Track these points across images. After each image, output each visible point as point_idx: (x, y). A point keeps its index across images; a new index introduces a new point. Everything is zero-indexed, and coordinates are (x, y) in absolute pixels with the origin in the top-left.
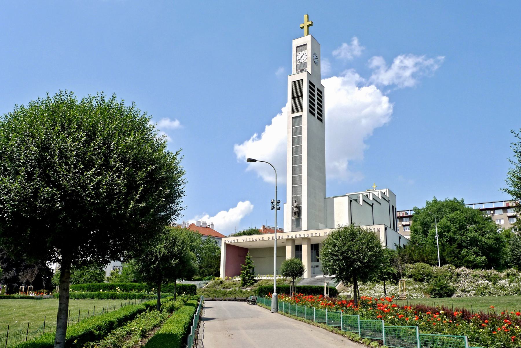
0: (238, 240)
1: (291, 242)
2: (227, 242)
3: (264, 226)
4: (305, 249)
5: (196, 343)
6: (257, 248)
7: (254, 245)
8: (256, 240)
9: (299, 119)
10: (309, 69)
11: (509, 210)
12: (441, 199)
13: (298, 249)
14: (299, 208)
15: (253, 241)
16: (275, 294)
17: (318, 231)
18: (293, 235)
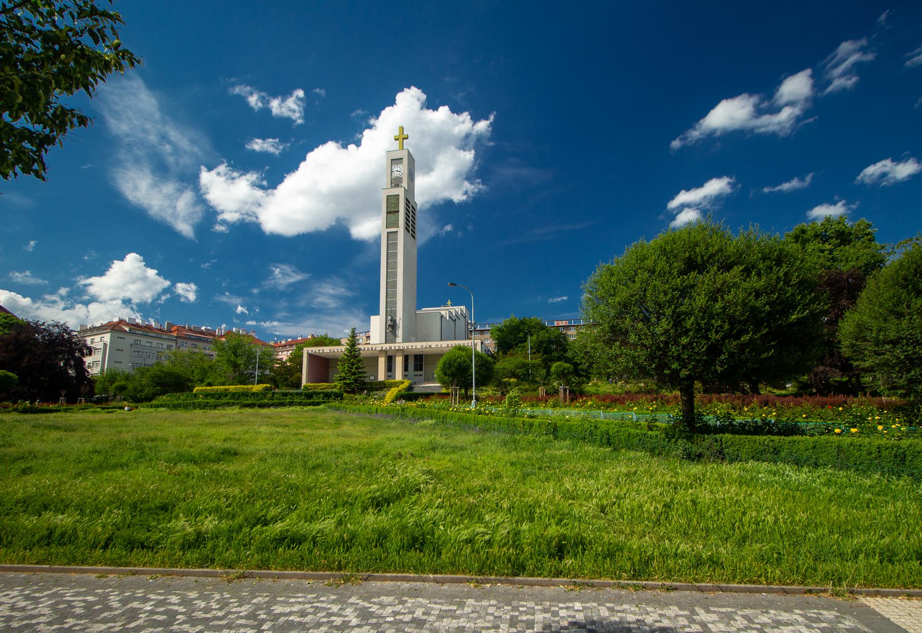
1: (384, 354)
2: (310, 352)
4: (399, 361)
7: (429, 351)
8: (315, 352)
10: (405, 184)
12: (329, 336)
13: (390, 360)
14: (394, 321)
16: (474, 401)
18: (387, 346)
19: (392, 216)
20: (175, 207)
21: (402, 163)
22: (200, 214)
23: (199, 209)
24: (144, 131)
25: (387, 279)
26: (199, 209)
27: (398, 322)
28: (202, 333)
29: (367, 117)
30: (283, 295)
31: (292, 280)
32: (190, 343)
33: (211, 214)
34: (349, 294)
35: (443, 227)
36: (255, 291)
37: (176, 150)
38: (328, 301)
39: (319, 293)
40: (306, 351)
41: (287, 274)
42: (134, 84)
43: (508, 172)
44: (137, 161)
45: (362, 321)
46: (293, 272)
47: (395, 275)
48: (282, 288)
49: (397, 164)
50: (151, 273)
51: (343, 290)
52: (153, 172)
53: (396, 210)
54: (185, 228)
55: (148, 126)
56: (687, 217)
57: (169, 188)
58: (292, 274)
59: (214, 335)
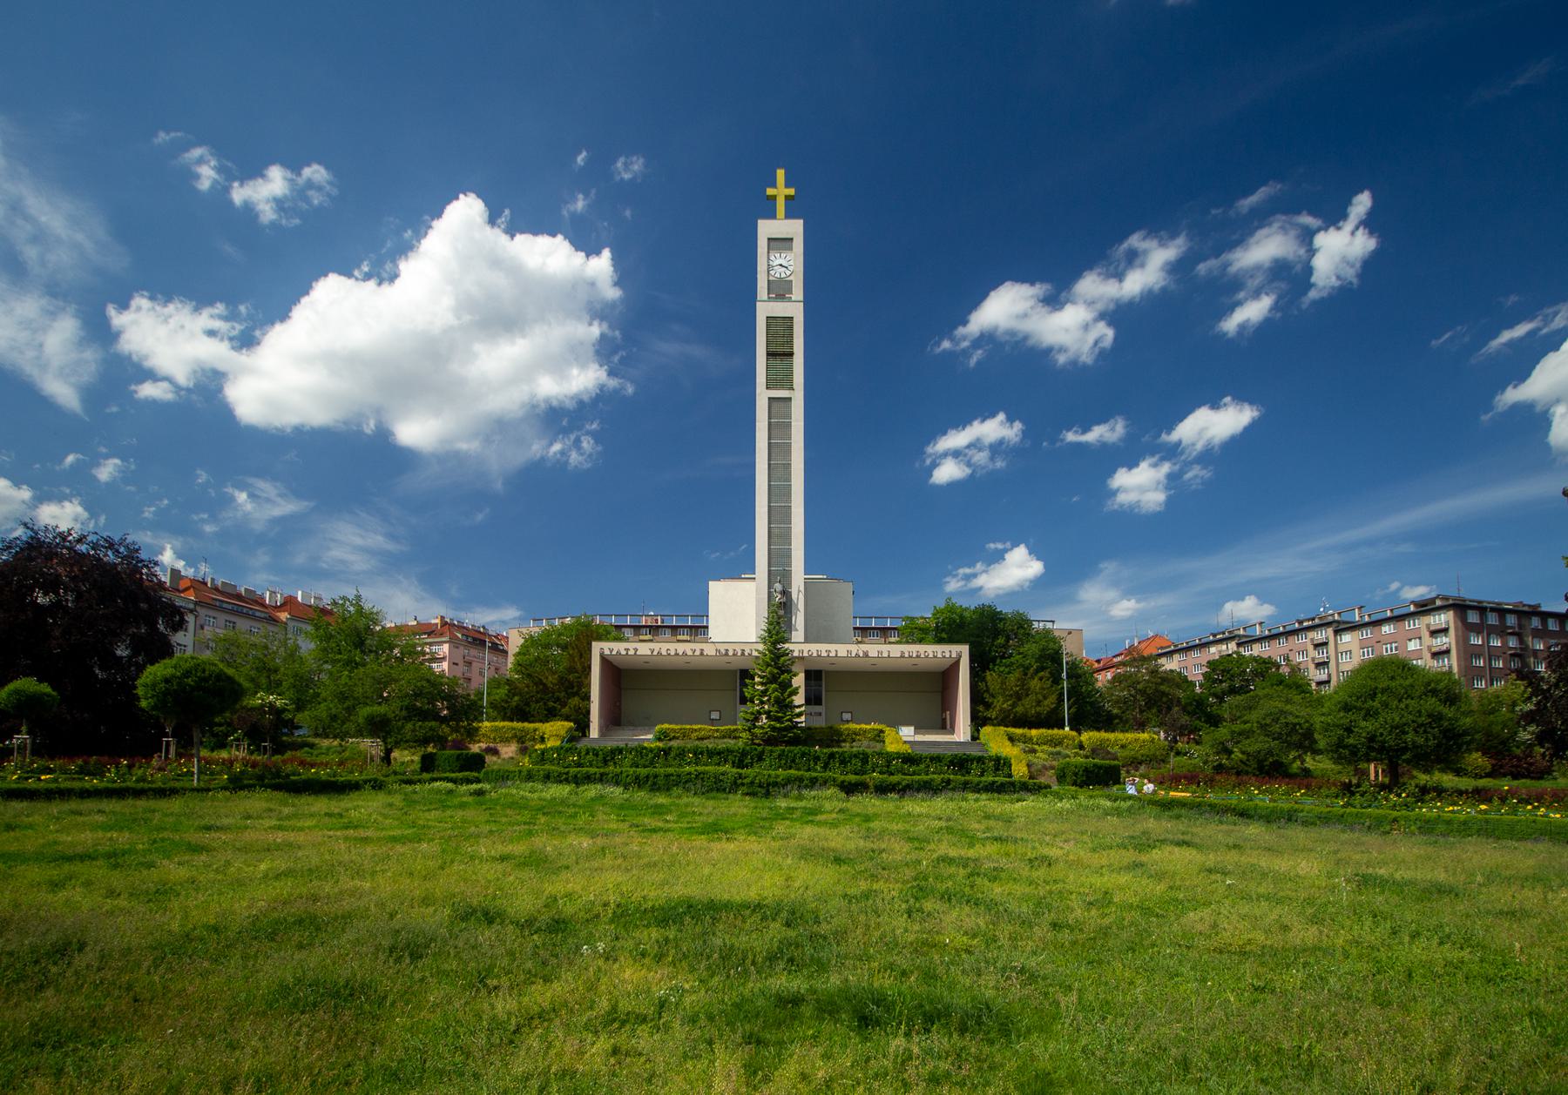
0: (636, 650)
2: (607, 652)
3: (442, 618)
6: (837, 672)
8: (685, 654)
9: (782, 404)
17: (833, 647)
19: (777, 362)
20: (41, 345)
22: (93, 367)
23: (91, 355)
25: (769, 502)
26: (91, 355)
27: (794, 596)
28: (239, 597)
31: (277, 512)
32: (222, 617)
34: (391, 546)
35: (551, 444)
37: (40, 237)
38: (351, 557)
39: (333, 540)
40: (597, 647)
41: (268, 500)
43: (667, 349)
46: (280, 495)
48: (258, 527)
49: (780, 250)
51: (380, 538)
54: (63, 392)
56: (947, 472)
58: (279, 499)
59: (263, 605)
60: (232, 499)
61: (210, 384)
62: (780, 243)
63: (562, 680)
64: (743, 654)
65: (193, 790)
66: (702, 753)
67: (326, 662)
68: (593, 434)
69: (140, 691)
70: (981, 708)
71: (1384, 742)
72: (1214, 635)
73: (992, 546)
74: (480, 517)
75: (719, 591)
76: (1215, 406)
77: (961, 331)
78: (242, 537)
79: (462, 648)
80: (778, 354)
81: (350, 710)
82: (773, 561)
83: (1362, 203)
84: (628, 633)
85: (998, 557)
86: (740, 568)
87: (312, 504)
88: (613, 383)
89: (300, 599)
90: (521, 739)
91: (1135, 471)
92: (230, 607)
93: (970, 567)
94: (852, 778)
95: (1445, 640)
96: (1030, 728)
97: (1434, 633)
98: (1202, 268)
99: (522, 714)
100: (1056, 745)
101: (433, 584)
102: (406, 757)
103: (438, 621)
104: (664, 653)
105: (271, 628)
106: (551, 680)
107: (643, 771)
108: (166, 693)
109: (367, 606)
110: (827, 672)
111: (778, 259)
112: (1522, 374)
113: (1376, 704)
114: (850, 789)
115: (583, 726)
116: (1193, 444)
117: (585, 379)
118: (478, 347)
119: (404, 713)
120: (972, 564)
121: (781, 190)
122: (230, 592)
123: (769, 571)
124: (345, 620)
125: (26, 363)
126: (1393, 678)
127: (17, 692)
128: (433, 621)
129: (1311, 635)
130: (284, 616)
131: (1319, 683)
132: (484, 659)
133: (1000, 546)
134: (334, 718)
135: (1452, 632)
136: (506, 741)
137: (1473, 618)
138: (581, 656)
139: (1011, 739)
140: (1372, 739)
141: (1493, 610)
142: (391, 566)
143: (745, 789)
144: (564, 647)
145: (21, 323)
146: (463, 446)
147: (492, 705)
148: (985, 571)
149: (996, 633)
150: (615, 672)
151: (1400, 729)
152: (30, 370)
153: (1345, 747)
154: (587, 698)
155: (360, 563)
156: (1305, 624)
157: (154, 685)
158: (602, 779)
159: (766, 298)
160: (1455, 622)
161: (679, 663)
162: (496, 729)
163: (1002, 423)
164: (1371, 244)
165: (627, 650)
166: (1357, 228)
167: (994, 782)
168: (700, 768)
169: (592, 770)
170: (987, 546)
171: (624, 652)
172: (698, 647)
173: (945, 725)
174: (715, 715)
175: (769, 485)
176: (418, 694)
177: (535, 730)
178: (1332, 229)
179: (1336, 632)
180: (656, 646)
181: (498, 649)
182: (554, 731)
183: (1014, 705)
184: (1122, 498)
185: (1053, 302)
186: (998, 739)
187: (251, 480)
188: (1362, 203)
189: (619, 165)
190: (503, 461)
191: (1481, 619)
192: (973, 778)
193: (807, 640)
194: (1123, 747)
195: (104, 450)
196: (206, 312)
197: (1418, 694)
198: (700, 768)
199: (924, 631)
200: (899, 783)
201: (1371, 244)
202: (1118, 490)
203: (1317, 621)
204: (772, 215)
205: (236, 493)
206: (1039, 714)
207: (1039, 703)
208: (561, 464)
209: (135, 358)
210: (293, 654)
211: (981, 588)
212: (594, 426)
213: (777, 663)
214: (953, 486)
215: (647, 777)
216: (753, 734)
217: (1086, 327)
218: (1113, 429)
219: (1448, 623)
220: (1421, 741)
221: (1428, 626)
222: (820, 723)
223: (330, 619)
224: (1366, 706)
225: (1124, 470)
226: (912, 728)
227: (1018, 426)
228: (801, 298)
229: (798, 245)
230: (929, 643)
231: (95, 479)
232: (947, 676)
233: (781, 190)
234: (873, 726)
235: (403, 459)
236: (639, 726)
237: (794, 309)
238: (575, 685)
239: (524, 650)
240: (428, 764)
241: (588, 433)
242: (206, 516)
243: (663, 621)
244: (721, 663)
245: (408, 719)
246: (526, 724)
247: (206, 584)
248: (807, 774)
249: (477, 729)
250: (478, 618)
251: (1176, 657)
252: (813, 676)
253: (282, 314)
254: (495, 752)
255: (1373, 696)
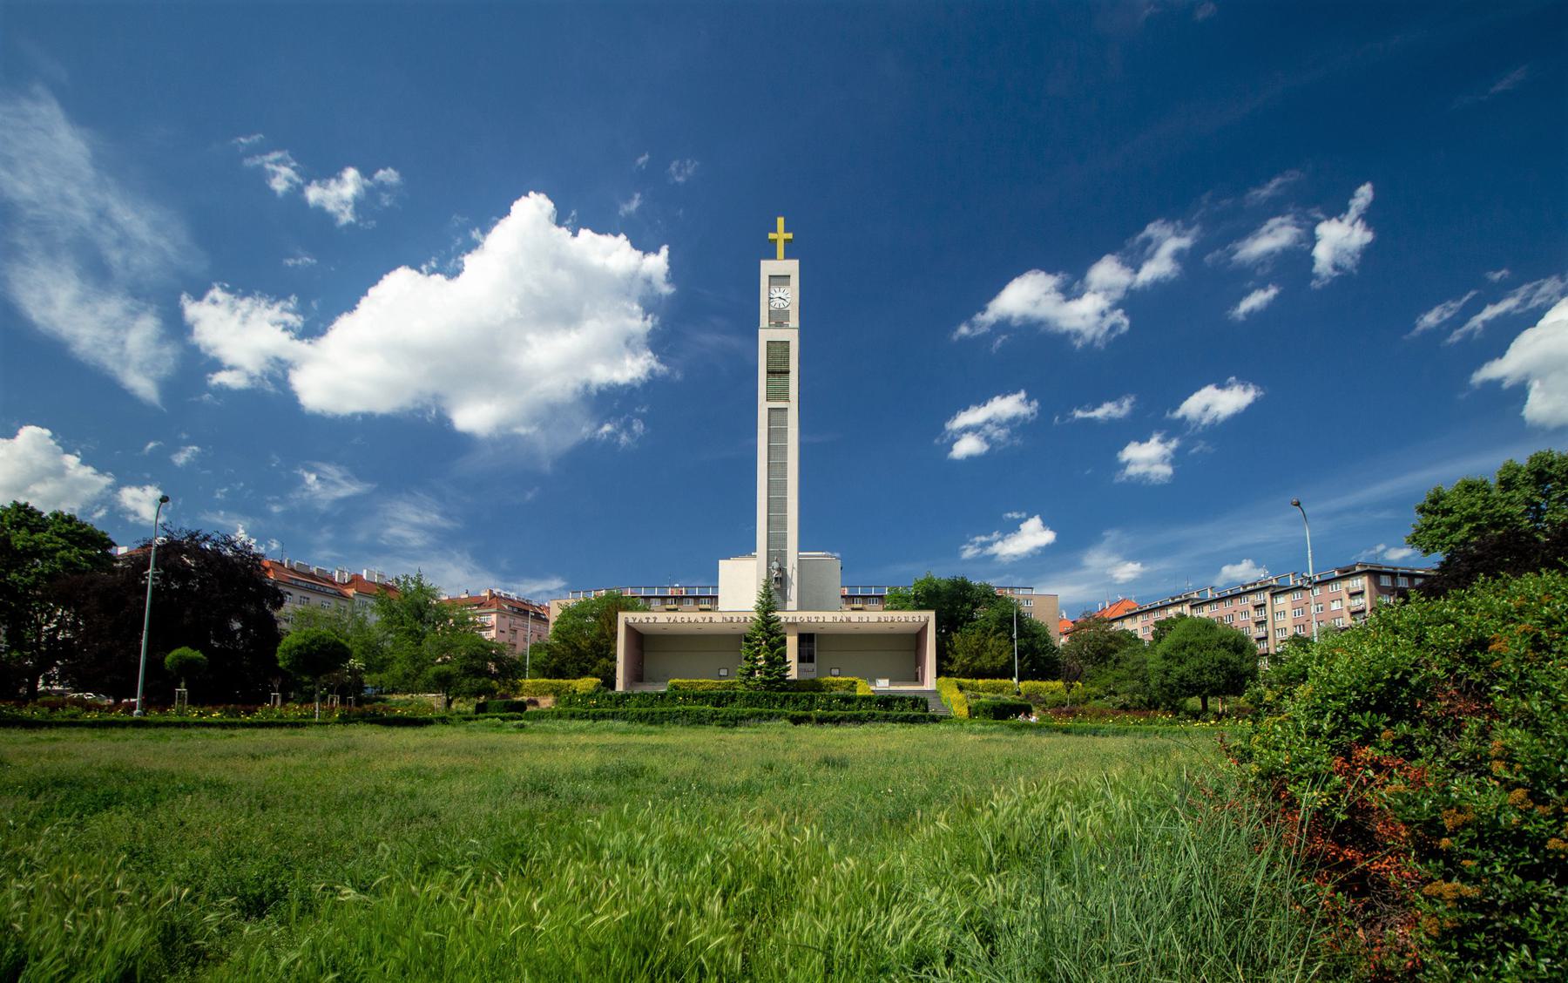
0: (655, 618)
2: (631, 621)
3: (491, 591)
5: (1215, 869)
6: (832, 635)
8: (641, 621)
11: (669, 600)
15: (690, 622)
19: (776, 379)
20: (123, 343)
21: (788, 284)
22: (171, 362)
23: (170, 351)
24: (65, 201)
26: (170, 351)
27: (789, 573)
28: (312, 576)
29: (465, 230)
30: (325, 518)
33: (198, 364)
34: (446, 524)
35: (601, 426)
36: (276, 509)
37: (124, 241)
39: (394, 519)
40: (623, 617)
41: (333, 483)
42: (44, 110)
44: (51, 251)
45: (469, 573)
46: (345, 478)
47: (783, 487)
48: (323, 507)
50: (72, 461)
51: (436, 517)
52: (82, 276)
53: (784, 369)
54: (143, 385)
55: (73, 191)
56: (967, 447)
57: (113, 307)
58: (342, 482)
59: (333, 583)
60: (302, 480)
61: (279, 371)
62: (780, 280)
63: (593, 645)
64: (745, 621)
65: (317, 724)
66: (689, 697)
67: (390, 632)
68: (645, 419)
69: (279, 655)
70: (945, 663)
71: (1189, 681)
72: (1173, 599)
73: (1009, 515)
74: (529, 496)
75: (727, 568)
76: (1222, 386)
77: (979, 317)
78: (310, 517)
79: (508, 617)
80: (778, 371)
81: (420, 670)
82: (771, 543)
83: (1364, 194)
84: (656, 604)
85: (1013, 528)
86: (745, 548)
87: (375, 486)
88: (662, 369)
89: (365, 577)
90: (556, 692)
91: (1145, 445)
92: (305, 585)
93: (986, 536)
94: (801, 713)
95: (1361, 601)
96: (977, 679)
97: (1352, 595)
98: (1208, 259)
99: (559, 673)
100: (998, 692)
101: (484, 559)
102: (463, 706)
103: (486, 594)
104: (679, 621)
105: (343, 603)
106: (584, 644)
107: (644, 710)
108: (298, 656)
109: (426, 582)
110: (821, 636)
111: (778, 292)
112: (1500, 352)
113: (1185, 654)
114: (797, 721)
115: (610, 682)
116: (1201, 419)
117: (633, 368)
118: (530, 337)
119: (462, 672)
120: (989, 534)
121: (781, 235)
122: (306, 572)
123: (768, 552)
124: (406, 596)
125: (108, 359)
126: (1198, 635)
127: (179, 657)
128: (483, 595)
129: (1252, 597)
130: (351, 592)
131: (1259, 640)
132: (527, 627)
133: (1016, 516)
134: (407, 676)
135: (1367, 594)
136: (545, 694)
137: (1386, 581)
138: (610, 624)
139: (961, 688)
140: (1181, 679)
141: (1403, 575)
142: (445, 542)
143: (719, 722)
144: (597, 617)
145: (105, 322)
146: (522, 430)
147: (534, 666)
148: (1002, 540)
149: (965, 600)
150: (639, 638)
151: (1200, 672)
152: (112, 365)
153: (1165, 686)
154: (614, 659)
155: (416, 540)
156: (1249, 588)
157: (290, 651)
158: (613, 716)
159: (767, 325)
160: (1369, 585)
161: (693, 629)
162: (536, 685)
163: (1021, 401)
164: (1368, 237)
165: (648, 618)
166: (1356, 221)
167: (908, 715)
168: (687, 707)
169: (606, 710)
170: (1005, 515)
171: (645, 621)
172: (707, 615)
173: (917, 678)
174: (724, 672)
175: (769, 481)
176: (474, 657)
177: (569, 685)
178: (1334, 220)
179: (1272, 595)
180: (678, 616)
181: (539, 618)
182: (586, 684)
183: (972, 661)
184: (1131, 470)
185: (1070, 292)
186: (950, 687)
187: (317, 464)
188: (1364, 194)
189: (673, 168)
190: (552, 444)
191: (1392, 581)
192: (893, 713)
193: (801, 608)
194: (1052, 693)
195: (184, 436)
196: (277, 308)
197: (1213, 646)
198: (687, 707)
199: (907, 599)
200: (835, 716)
201: (1368, 237)
202: (1128, 462)
203: (1258, 586)
204: (773, 256)
205: (306, 475)
206: (994, 668)
207: (993, 658)
208: (611, 442)
209: (203, 349)
210: (361, 626)
211: (996, 555)
212: (644, 410)
213: (769, 631)
214: (971, 459)
215: (647, 714)
216: (748, 686)
217: (1103, 314)
218: (1120, 407)
219: (1363, 586)
220: (1213, 679)
221: (1347, 589)
222: (808, 676)
223: (392, 595)
224: (1179, 655)
225: (1136, 443)
226: (887, 681)
227: (1035, 403)
228: (797, 325)
229: (795, 281)
230: (910, 610)
231: (171, 463)
232: (918, 637)
233: (781, 235)
234: (850, 679)
235: (464, 443)
236: (660, 681)
237: (791, 335)
238: (604, 648)
239: (561, 620)
240: (481, 708)
241: (639, 416)
242: (277, 498)
243: (687, 592)
244: (728, 629)
245: (465, 676)
246: (561, 681)
247: (283, 565)
248: (766, 710)
249: (521, 685)
250: (525, 590)
251: (1140, 618)
252: (806, 639)
253: (349, 304)
254: (535, 703)
255: (1184, 648)
